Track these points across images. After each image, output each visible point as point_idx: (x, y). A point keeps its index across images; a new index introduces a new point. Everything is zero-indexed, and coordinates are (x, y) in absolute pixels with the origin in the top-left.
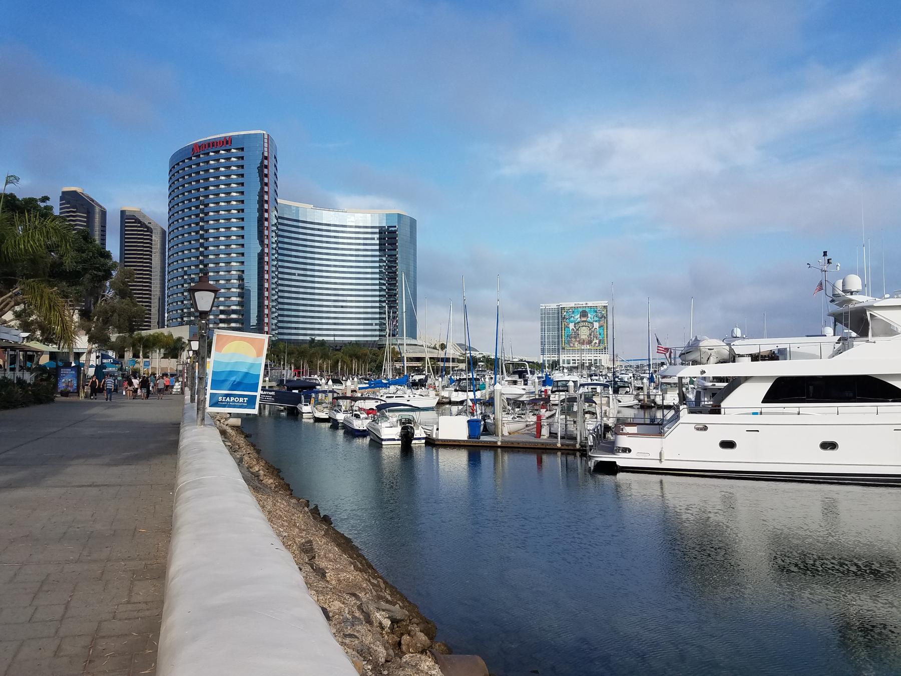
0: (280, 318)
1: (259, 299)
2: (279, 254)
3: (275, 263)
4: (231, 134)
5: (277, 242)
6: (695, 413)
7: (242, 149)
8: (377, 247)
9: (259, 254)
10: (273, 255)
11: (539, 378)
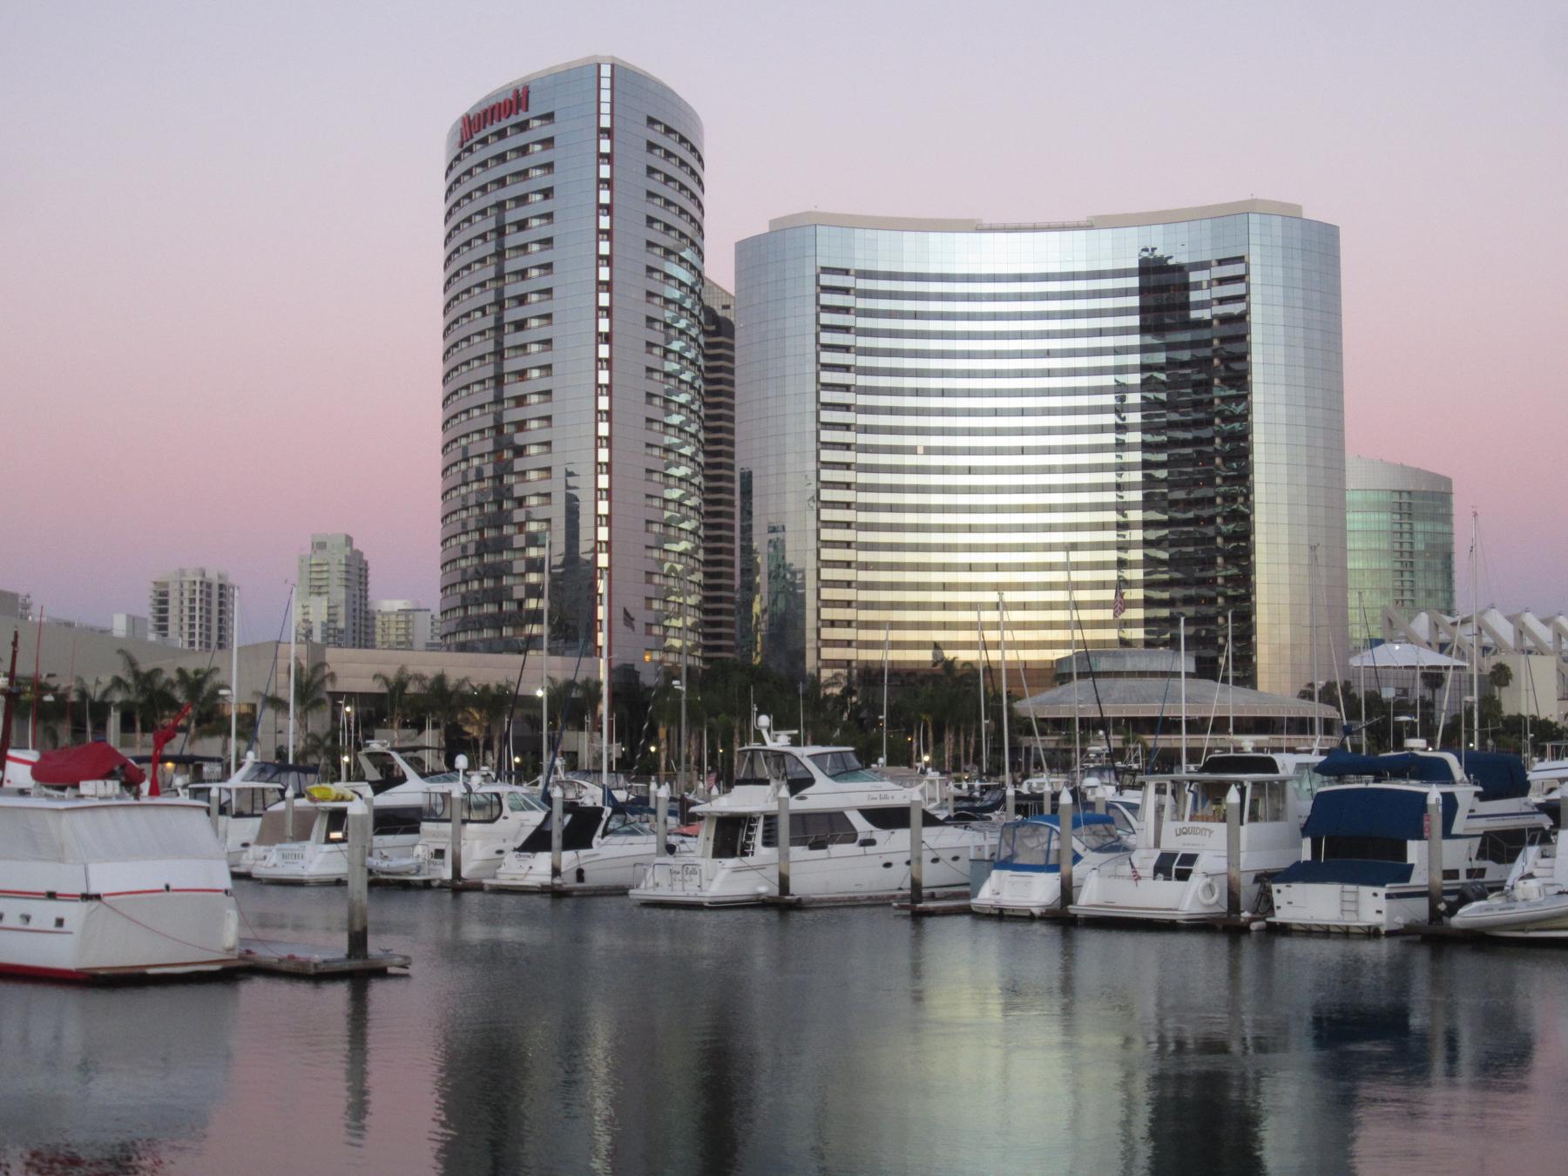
8: (1134, 301)
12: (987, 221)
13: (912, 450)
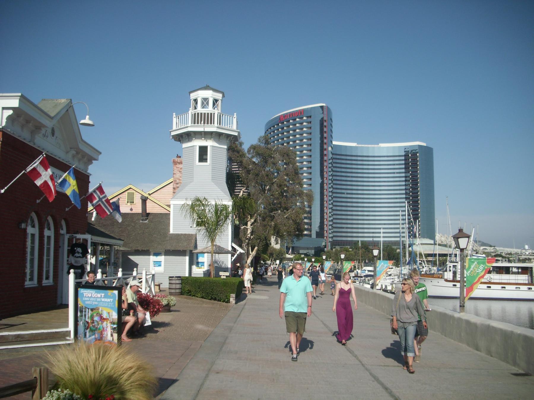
0: (334, 221)
1: (321, 188)
2: (333, 171)
3: (331, 190)
4: (363, 146)
5: (332, 175)
6: (97, 151)
7: (310, 117)
8: (403, 166)
9: (321, 184)
10: (330, 184)
11: (347, 283)
12: (320, 181)
13: (344, 193)
